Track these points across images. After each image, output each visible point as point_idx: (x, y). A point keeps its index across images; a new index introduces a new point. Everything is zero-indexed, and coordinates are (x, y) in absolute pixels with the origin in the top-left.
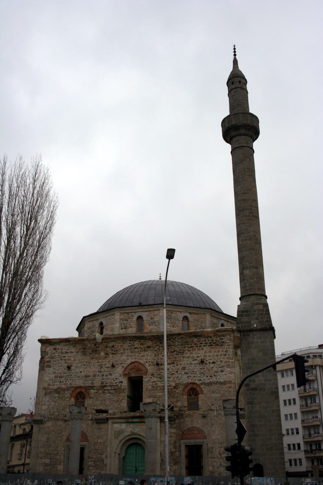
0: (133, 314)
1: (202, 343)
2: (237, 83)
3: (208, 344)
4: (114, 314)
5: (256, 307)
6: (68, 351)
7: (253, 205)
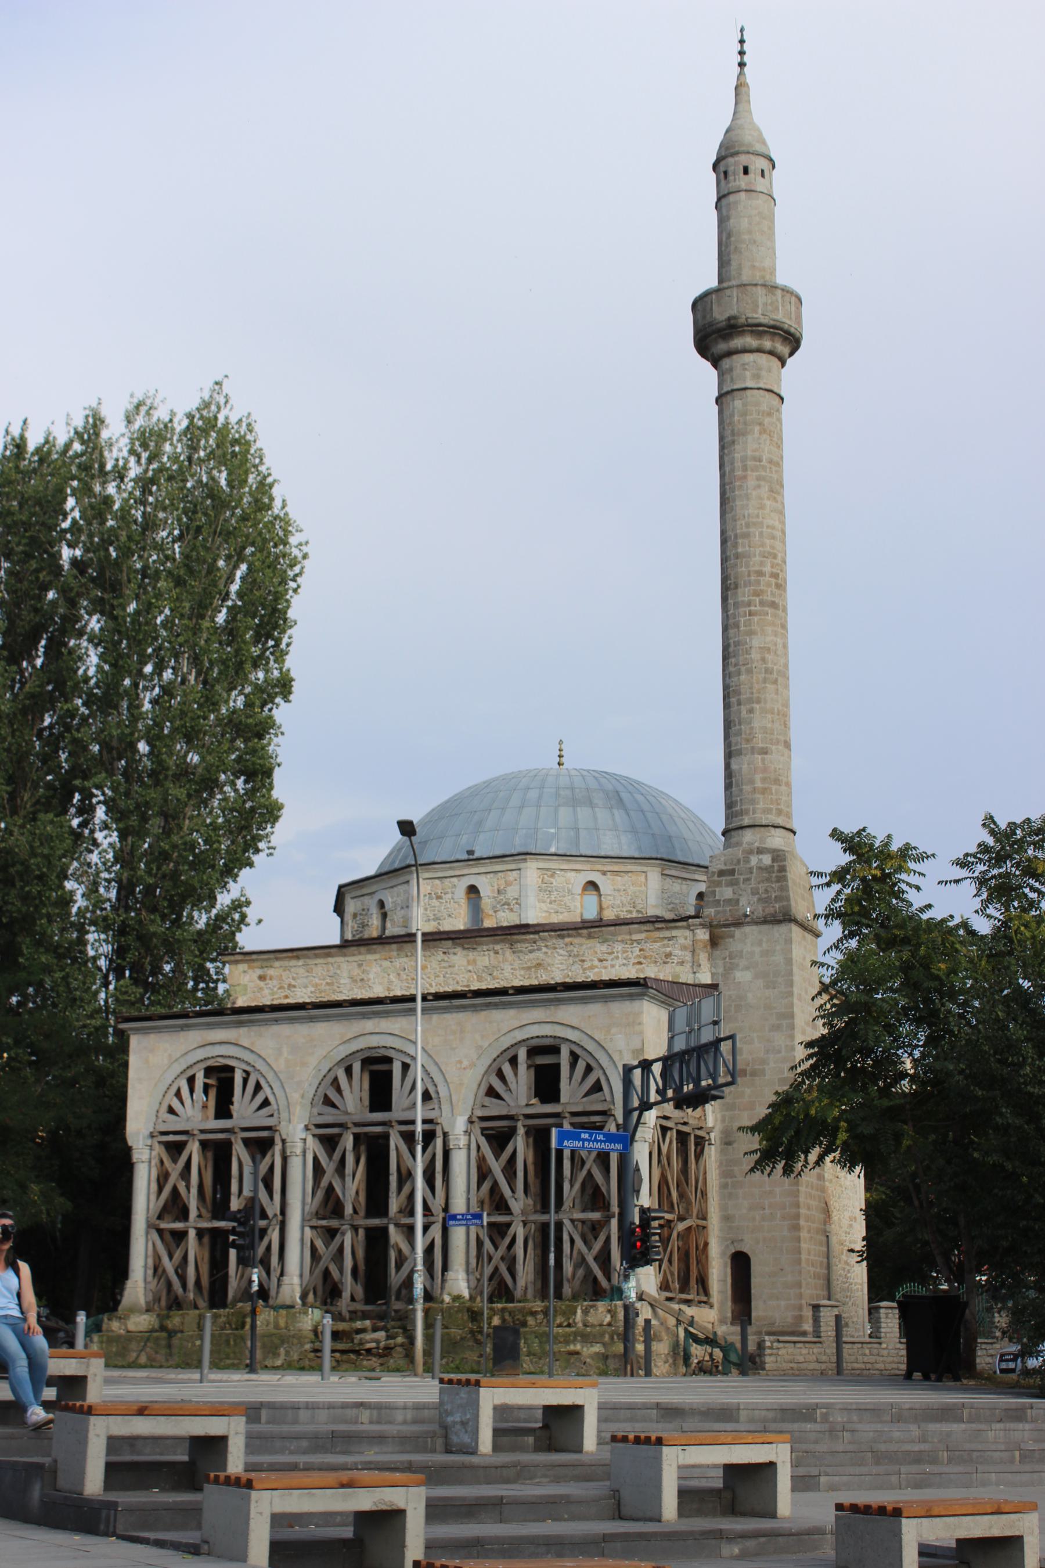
0: (455, 880)
1: (617, 958)
2: (736, 166)
3: (633, 961)
4: (408, 882)
5: (754, 860)
6: (293, 983)
7: (764, 569)
